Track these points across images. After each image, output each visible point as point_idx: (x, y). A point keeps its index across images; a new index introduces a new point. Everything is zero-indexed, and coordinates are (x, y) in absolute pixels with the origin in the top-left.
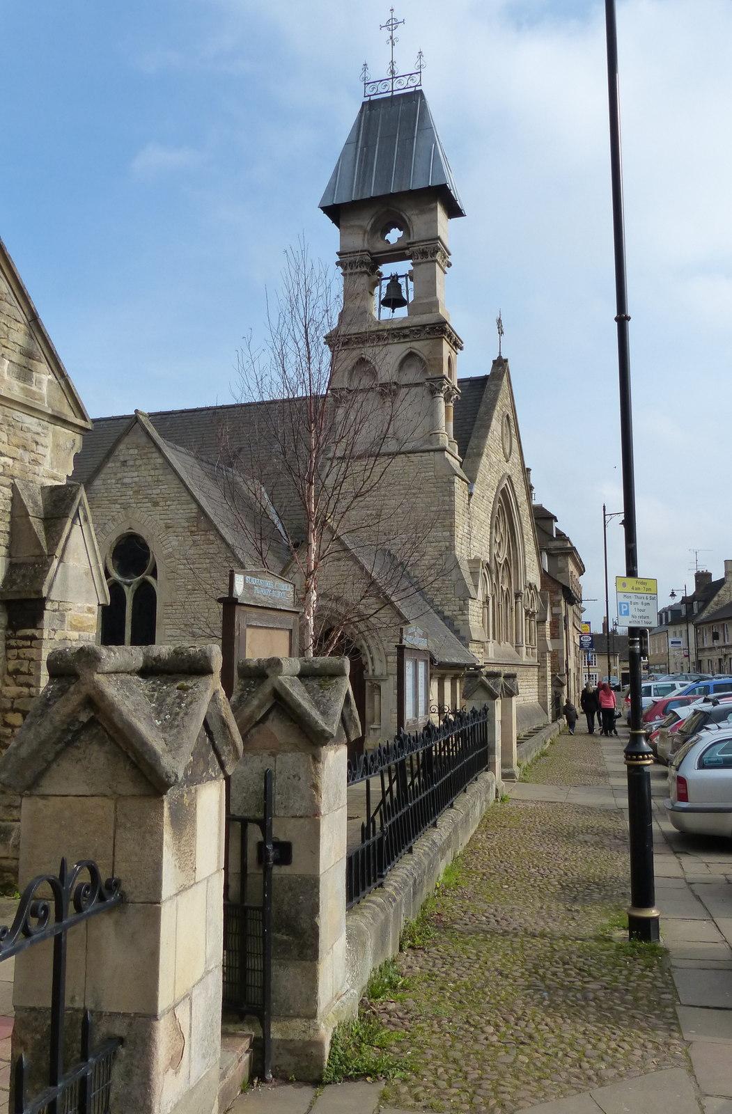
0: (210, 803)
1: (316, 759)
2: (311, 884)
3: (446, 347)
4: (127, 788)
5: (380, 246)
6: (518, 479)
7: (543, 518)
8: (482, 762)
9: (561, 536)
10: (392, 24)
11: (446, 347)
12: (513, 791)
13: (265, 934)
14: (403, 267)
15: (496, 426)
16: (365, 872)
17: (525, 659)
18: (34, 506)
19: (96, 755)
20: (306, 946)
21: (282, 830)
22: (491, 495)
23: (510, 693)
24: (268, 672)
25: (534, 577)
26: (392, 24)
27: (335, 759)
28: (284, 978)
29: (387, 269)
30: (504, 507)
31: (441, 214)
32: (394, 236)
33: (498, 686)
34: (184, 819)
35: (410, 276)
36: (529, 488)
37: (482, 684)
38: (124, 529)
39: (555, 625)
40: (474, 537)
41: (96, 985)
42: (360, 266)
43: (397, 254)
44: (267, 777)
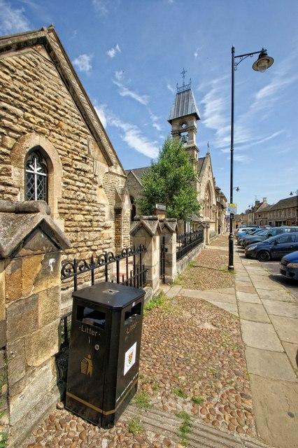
0: (158, 239)
1: (172, 235)
2: (171, 255)
3: (195, 152)
4: (147, 236)
5: (181, 129)
6: (211, 181)
7: (217, 190)
8: (202, 241)
9: (222, 193)
10: (184, 72)
11: (195, 152)
12: (207, 247)
13: (165, 263)
14: (187, 133)
15: (207, 169)
16: (179, 256)
17: (212, 221)
18: (119, 191)
19: (142, 231)
20: (170, 265)
21: (166, 246)
22: (205, 185)
23: (208, 228)
24: (157, 212)
25: (215, 203)
26: (184, 72)
27: (175, 235)
28: (167, 269)
29: (182, 134)
30: (208, 188)
31: (195, 119)
32: (184, 126)
33: (205, 226)
34: (155, 240)
35: (187, 135)
36: (214, 183)
37: (204, 226)
38: (38, 144)
39: (219, 213)
40: (201, 195)
41: (145, 262)
42: (177, 133)
43: (185, 130)
44: (164, 238)
